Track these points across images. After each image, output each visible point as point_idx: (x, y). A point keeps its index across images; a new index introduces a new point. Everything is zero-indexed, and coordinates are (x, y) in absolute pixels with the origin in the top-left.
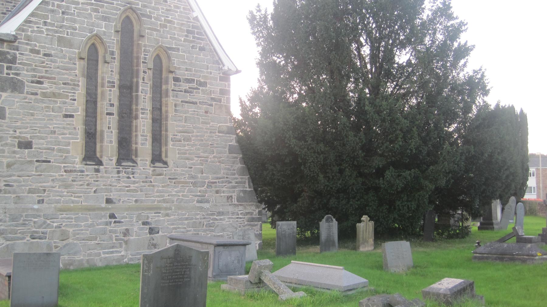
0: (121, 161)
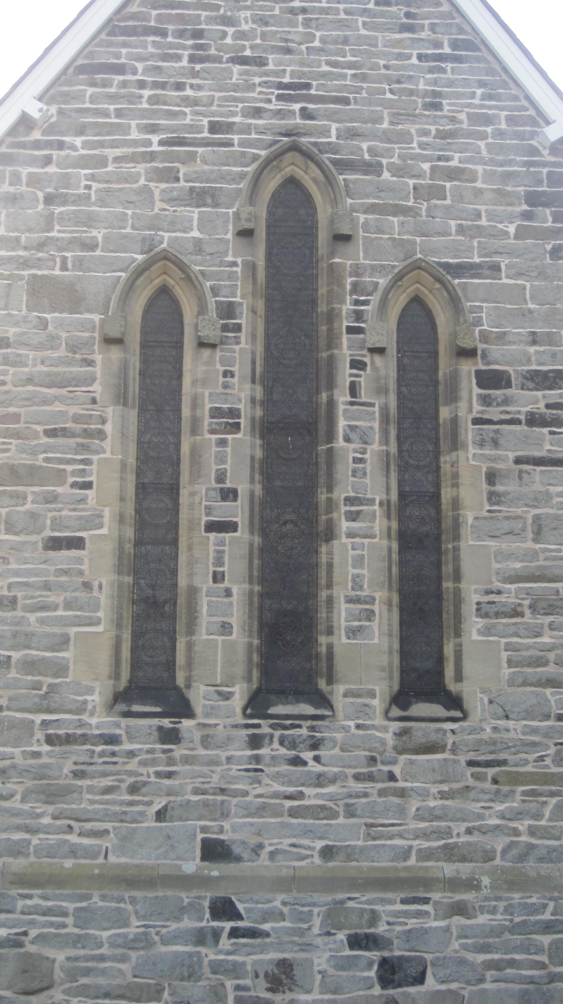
0: (273, 697)
